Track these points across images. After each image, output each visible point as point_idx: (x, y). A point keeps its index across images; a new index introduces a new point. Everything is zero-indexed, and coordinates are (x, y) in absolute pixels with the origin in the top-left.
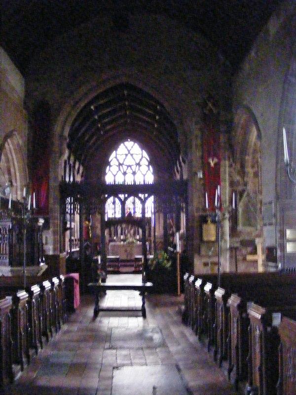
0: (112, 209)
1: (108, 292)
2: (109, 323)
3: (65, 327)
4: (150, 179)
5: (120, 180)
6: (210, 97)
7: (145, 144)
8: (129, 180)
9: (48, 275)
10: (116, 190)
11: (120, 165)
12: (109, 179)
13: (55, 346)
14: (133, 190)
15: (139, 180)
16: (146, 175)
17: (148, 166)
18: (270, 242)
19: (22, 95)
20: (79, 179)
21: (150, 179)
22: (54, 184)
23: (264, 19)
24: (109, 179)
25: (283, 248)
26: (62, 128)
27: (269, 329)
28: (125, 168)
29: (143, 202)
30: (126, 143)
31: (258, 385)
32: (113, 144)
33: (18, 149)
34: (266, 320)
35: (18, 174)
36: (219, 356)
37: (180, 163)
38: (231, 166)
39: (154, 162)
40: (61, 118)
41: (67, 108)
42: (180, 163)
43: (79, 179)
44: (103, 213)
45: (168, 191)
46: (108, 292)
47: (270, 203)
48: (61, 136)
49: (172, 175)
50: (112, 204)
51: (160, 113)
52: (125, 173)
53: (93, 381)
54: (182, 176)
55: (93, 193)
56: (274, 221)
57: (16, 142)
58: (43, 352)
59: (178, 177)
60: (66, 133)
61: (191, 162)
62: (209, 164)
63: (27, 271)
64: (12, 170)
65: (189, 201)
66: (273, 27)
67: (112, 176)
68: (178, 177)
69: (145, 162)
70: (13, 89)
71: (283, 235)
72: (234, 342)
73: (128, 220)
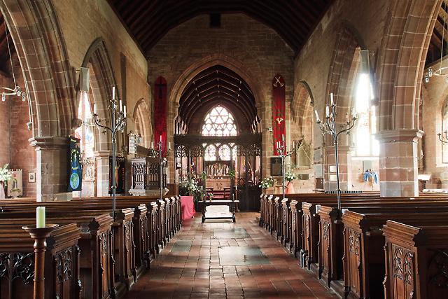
0: (210, 155)
1: (207, 208)
2: (209, 226)
3: (182, 229)
4: (234, 133)
5: (213, 133)
6: (278, 76)
7: (231, 109)
8: (219, 134)
9: (168, 195)
10: (212, 140)
11: (213, 123)
12: (205, 133)
13: (179, 237)
14: (225, 140)
15: (226, 133)
16: (232, 131)
17: (233, 124)
18: (319, 175)
19: (146, 73)
20: (184, 132)
21: (234, 133)
22: (170, 136)
23: (318, 18)
24: (205, 133)
25: (327, 179)
26: (175, 96)
27: (314, 215)
28: (216, 126)
29: (231, 148)
30: (217, 108)
31: (308, 249)
32: (206, 108)
33: (145, 111)
34: (312, 210)
35: (145, 129)
36: (284, 241)
37: (256, 122)
38: (292, 123)
39: (237, 122)
40: (174, 90)
41: (178, 83)
42: (256, 122)
43: (184, 132)
44: (203, 157)
45: (249, 141)
46: (207, 208)
47: (319, 148)
48: (174, 103)
49: (249, 129)
50: (92, 150)
51: (242, 86)
52: (216, 130)
53: (183, 282)
54: (257, 131)
55: (192, 142)
56: (321, 160)
57: (143, 107)
58: (172, 240)
59: (254, 132)
60: (178, 101)
61: (264, 121)
62: (277, 122)
63: (155, 193)
64: (141, 127)
65: (263, 147)
66: (325, 23)
67: (207, 131)
68: (254, 132)
69: (230, 121)
70: (140, 68)
71: (327, 168)
72: (293, 230)
73: (219, 162)
